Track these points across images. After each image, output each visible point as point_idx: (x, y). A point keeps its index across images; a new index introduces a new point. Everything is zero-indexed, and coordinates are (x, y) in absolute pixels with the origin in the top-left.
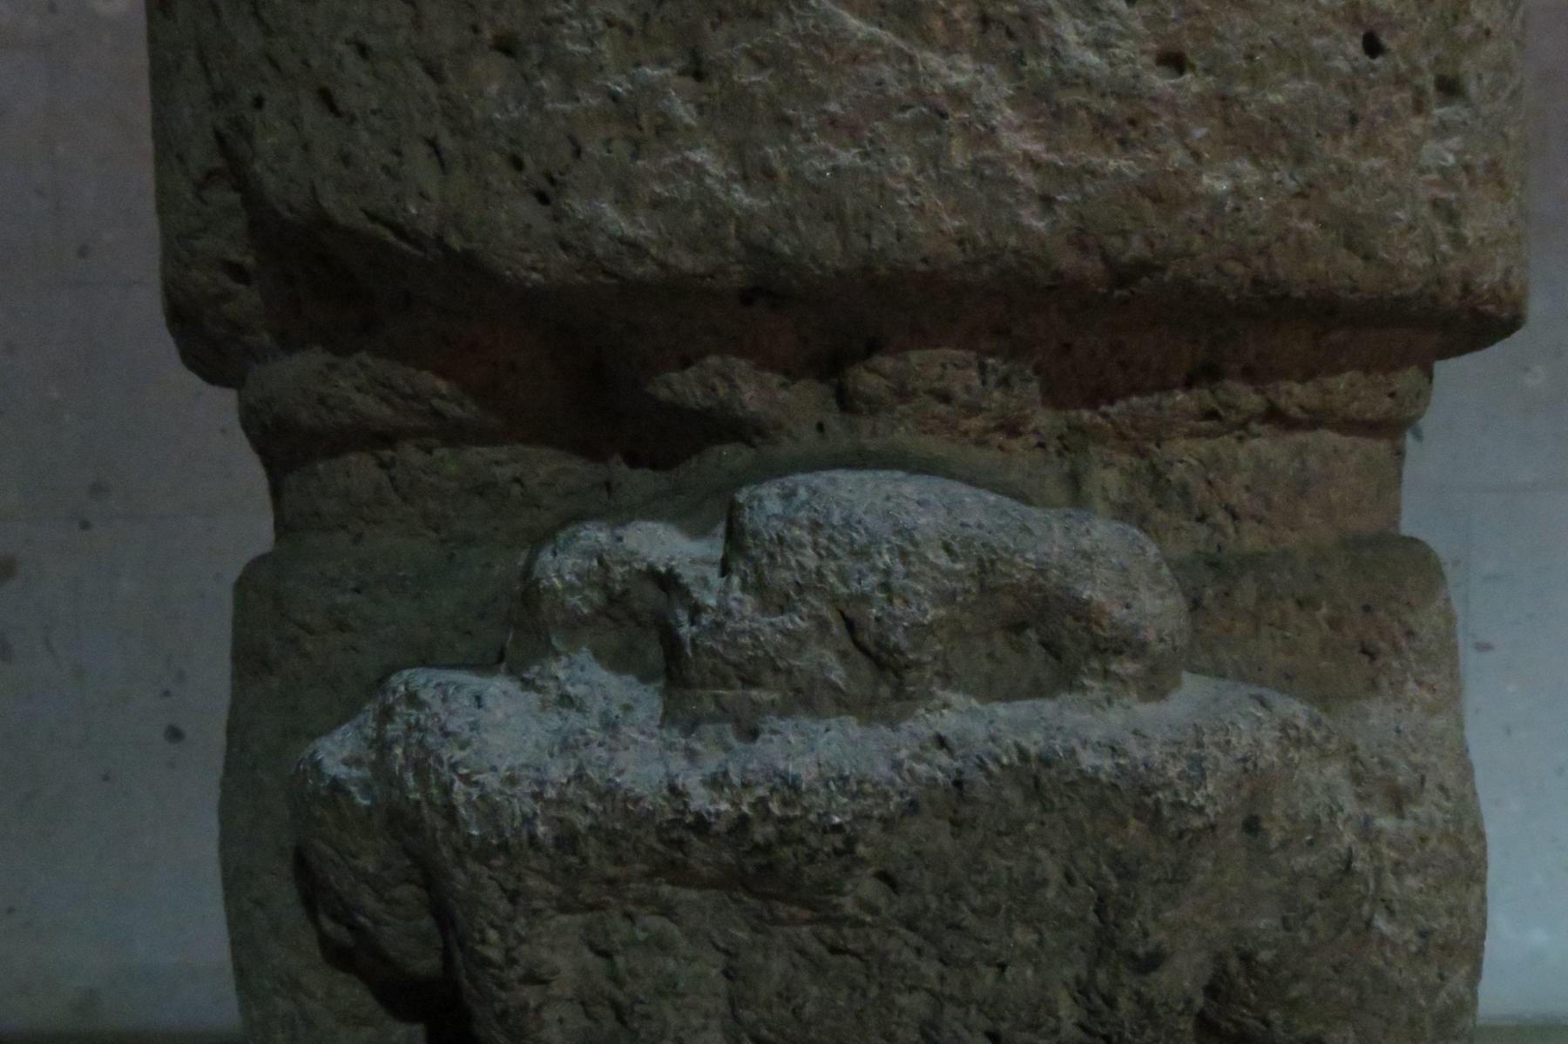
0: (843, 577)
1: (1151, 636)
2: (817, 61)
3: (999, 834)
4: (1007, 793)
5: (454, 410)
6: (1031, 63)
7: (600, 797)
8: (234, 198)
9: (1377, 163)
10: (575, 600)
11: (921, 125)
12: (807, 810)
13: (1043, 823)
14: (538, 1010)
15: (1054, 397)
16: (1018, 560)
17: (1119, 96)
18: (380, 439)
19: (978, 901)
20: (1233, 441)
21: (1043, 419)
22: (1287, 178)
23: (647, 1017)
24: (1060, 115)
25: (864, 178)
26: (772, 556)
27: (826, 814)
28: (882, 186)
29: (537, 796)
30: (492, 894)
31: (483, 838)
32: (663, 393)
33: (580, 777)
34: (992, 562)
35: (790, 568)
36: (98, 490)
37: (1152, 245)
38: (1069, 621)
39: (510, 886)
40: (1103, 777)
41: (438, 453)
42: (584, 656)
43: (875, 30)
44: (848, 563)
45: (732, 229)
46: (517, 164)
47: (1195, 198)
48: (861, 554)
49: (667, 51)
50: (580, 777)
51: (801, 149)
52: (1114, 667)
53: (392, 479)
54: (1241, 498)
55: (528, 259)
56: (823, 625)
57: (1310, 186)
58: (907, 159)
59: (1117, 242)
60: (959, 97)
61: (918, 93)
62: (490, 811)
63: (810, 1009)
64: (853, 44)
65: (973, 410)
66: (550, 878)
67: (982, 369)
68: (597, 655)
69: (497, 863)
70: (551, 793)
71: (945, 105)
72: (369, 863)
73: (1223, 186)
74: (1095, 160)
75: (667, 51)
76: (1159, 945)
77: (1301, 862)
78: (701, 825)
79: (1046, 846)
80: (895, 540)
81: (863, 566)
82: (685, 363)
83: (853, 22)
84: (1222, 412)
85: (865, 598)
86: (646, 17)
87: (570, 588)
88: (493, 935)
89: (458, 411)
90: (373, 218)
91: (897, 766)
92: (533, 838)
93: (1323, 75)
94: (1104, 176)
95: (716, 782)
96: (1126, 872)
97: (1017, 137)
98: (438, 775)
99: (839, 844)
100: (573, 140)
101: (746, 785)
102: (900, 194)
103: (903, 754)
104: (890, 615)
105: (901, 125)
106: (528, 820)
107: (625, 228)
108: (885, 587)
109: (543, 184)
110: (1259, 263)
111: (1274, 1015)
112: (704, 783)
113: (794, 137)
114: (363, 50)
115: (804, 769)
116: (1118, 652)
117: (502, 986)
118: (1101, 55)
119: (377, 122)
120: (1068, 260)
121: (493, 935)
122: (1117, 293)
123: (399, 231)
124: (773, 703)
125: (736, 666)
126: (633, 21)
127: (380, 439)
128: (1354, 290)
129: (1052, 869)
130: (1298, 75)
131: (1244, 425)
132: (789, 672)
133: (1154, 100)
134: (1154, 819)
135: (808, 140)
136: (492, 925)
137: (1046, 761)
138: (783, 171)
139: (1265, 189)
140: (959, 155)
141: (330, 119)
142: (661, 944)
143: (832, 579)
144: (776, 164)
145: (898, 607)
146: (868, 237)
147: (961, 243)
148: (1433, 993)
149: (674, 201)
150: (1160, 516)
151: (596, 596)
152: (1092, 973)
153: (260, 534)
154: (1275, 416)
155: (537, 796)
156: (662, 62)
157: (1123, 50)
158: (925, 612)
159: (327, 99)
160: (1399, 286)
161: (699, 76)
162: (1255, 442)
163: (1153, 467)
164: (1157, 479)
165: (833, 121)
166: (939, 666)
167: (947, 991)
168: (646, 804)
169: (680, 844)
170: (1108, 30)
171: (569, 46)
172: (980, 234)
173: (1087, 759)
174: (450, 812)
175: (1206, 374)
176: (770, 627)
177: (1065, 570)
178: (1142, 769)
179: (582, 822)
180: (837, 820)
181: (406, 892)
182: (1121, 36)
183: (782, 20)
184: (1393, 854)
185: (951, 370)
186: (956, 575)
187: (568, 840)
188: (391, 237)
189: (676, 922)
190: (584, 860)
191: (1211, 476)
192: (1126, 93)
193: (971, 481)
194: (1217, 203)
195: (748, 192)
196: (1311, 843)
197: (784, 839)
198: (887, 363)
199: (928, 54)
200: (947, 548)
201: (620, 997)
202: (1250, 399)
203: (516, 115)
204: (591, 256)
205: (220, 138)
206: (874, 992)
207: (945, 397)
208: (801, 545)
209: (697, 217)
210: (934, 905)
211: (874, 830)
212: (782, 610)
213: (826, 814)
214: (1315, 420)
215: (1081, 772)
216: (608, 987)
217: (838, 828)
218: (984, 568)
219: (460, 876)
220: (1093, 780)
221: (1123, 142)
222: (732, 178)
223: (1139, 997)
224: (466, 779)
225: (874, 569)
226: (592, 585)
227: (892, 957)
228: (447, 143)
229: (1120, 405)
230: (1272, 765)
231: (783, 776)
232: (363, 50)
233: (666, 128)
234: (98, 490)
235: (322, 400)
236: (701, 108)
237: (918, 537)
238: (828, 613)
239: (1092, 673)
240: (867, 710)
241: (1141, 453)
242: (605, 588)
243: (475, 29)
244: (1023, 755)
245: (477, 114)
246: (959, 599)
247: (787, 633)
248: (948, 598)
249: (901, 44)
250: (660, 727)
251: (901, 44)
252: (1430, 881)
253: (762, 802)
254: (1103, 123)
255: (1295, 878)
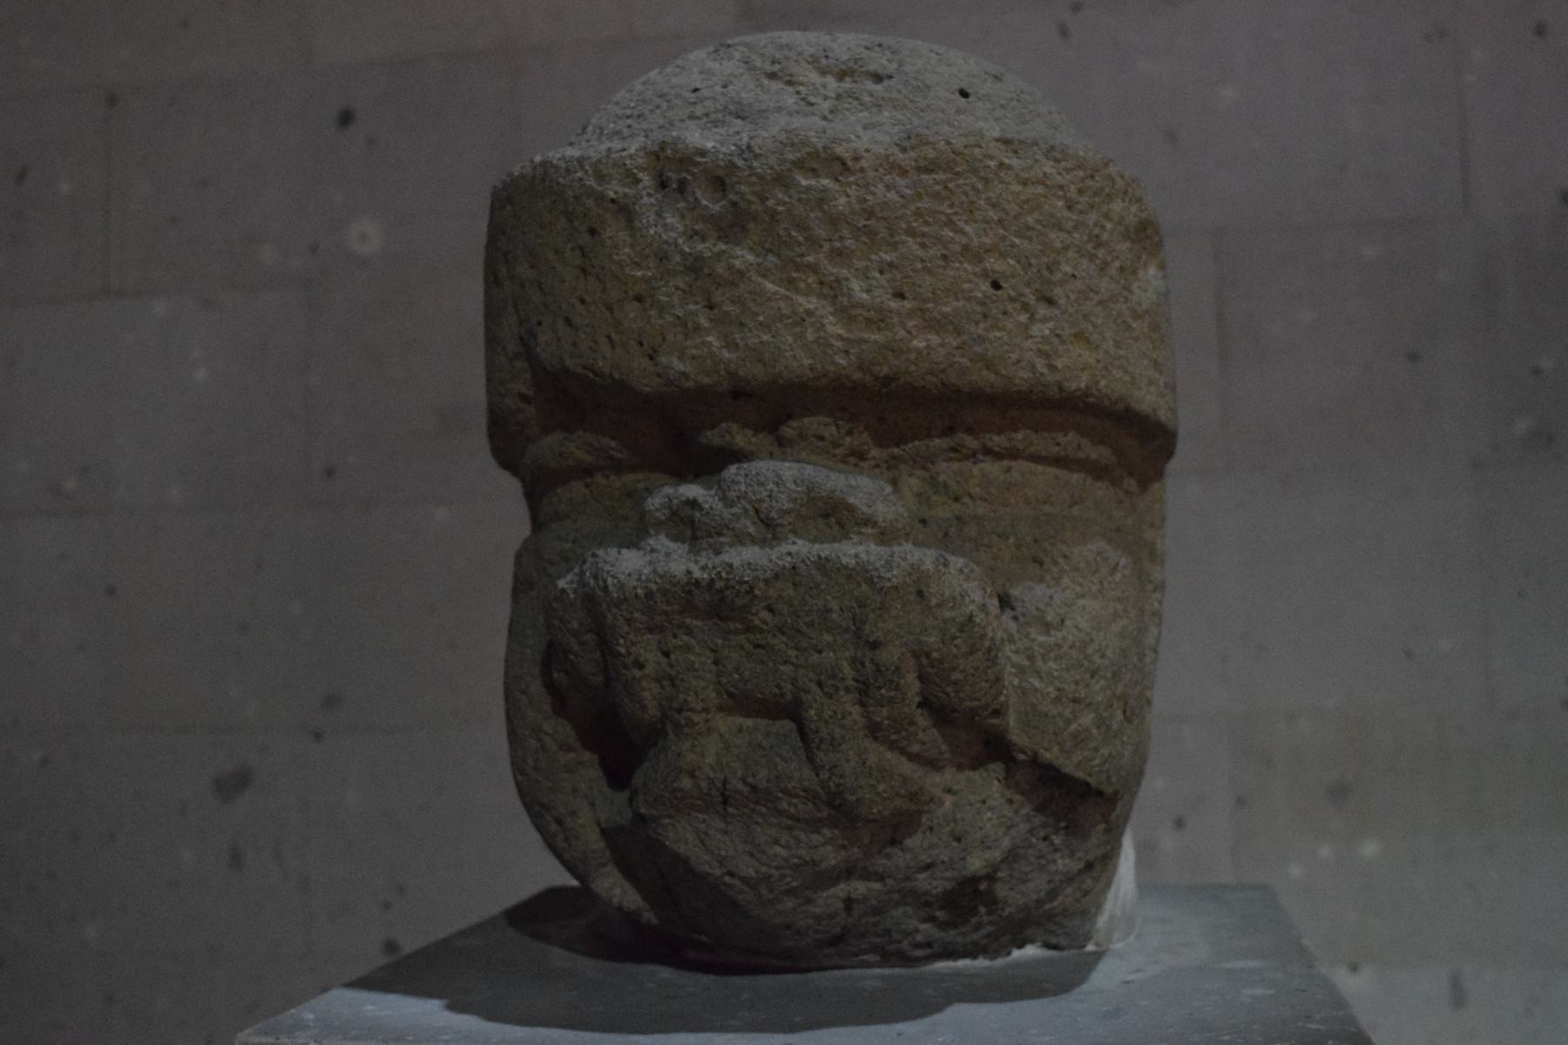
0: (754, 493)
1: (881, 519)
2: (754, 301)
3: (811, 588)
4: (813, 572)
5: (618, 455)
6: (840, 299)
7: (661, 577)
8: (526, 365)
9: (998, 334)
10: (658, 514)
11: (795, 324)
12: (735, 576)
13: (828, 585)
14: (640, 679)
15: (880, 442)
16: (823, 487)
17: (875, 310)
18: (587, 472)
19: (807, 619)
20: (971, 464)
21: (875, 452)
22: (953, 341)
23: (682, 680)
24: (852, 319)
25: (772, 345)
26: (729, 487)
27: (742, 576)
28: (779, 348)
29: (638, 580)
30: (621, 621)
31: (618, 597)
32: (704, 440)
33: (655, 571)
34: (813, 488)
35: (735, 491)
36: (331, 702)
37: (891, 369)
38: (845, 512)
39: (628, 617)
40: (851, 566)
41: (612, 478)
42: (662, 537)
43: (778, 288)
44: (756, 488)
45: (722, 366)
46: (641, 344)
47: (909, 350)
48: (762, 484)
49: (699, 299)
50: (655, 571)
51: (748, 335)
52: (863, 530)
53: (591, 492)
54: (976, 491)
55: (644, 381)
56: (746, 510)
57: (963, 344)
58: (789, 338)
59: (878, 368)
60: (809, 313)
61: (794, 312)
62: (621, 586)
63: (747, 673)
64: (769, 295)
65: (836, 445)
66: (643, 613)
67: (837, 426)
68: (667, 536)
69: (624, 607)
70: (644, 578)
71: (804, 316)
72: (575, 625)
73: (922, 345)
74: (866, 336)
75: (699, 299)
76: (878, 637)
77: (948, 614)
78: (697, 583)
79: (830, 594)
80: (776, 479)
81: (762, 489)
82: (713, 427)
83: (769, 286)
84: (959, 448)
85: (761, 501)
86: (691, 286)
87: (658, 510)
88: (621, 641)
89: (620, 456)
90: (585, 367)
91: (771, 561)
92: (636, 594)
93: (968, 299)
94: (868, 342)
95: (703, 568)
96: (862, 605)
97: (833, 328)
98: (602, 576)
99: (748, 589)
100: (662, 334)
101: (714, 568)
102: (786, 350)
103: (773, 557)
104: (771, 506)
105: (786, 325)
106: (635, 588)
107: (681, 367)
108: (770, 496)
109: (651, 352)
110: (942, 376)
111: (949, 689)
112: (699, 569)
113: (746, 330)
114: (583, 301)
115: (736, 562)
116: (866, 525)
117: (625, 666)
118: (868, 295)
119: (587, 330)
120: (857, 376)
121: (621, 641)
122: (884, 390)
123: (596, 374)
124: (728, 543)
125: (714, 528)
126: (686, 289)
127: (587, 472)
128: (992, 387)
129: (834, 605)
130: (957, 299)
131: (974, 455)
132: (733, 529)
133: (890, 312)
134: (870, 581)
135: (751, 331)
136: (622, 637)
137: (827, 559)
138: (741, 344)
139: (942, 345)
140: (810, 335)
141: (568, 329)
142: (687, 648)
143: (750, 494)
144: (738, 341)
145: (774, 503)
146: (774, 367)
147: (811, 369)
148: (1068, 722)
149: (700, 357)
150: (935, 498)
151: (666, 512)
152: (856, 653)
153: (526, 530)
154: (988, 451)
155: (638, 580)
156: (697, 303)
157: (877, 292)
158: (784, 505)
159: (568, 321)
160: (1016, 385)
161: (711, 308)
162: (982, 465)
163: (931, 477)
164: (933, 481)
165: (761, 324)
166: (790, 527)
167: (799, 663)
168: (678, 578)
169: (689, 592)
170: (870, 285)
171: (661, 297)
172: (819, 366)
173: (845, 560)
174: (606, 588)
175: (949, 431)
176: (727, 514)
177: (842, 491)
178: (866, 564)
179: (654, 587)
180: (746, 579)
181: (589, 637)
182: (876, 287)
183: (742, 286)
184: (1042, 651)
185: (822, 427)
186: (797, 492)
187: (649, 595)
188: (591, 375)
189: (693, 638)
190: (656, 602)
191: (958, 478)
192: (880, 310)
193: (808, 463)
194: (919, 352)
195: (729, 352)
196: (952, 607)
197: (727, 588)
198: (794, 424)
199: (798, 297)
200: (795, 482)
201: (673, 673)
202: (972, 443)
203: (640, 325)
204: (668, 379)
205: (521, 338)
206: (771, 664)
207: (822, 439)
208: (740, 483)
209: (709, 362)
210: (789, 621)
211: (762, 585)
212: (732, 507)
213: (742, 576)
214: (1014, 454)
215: (841, 564)
216: (668, 669)
217: (746, 582)
218: (809, 490)
219: (609, 616)
220: (846, 567)
221: (879, 328)
222: (723, 347)
223: (872, 661)
224: (613, 577)
225: (766, 490)
226: (665, 508)
227: (777, 647)
228: (614, 336)
229: (910, 445)
230: (928, 570)
231: (727, 564)
232: (583, 301)
233: (697, 328)
234: (331, 702)
235: (561, 454)
236: (711, 320)
237: (784, 478)
238: (748, 507)
239: (854, 532)
240: (763, 543)
241: (925, 469)
242: (670, 508)
243: (626, 292)
244: (820, 557)
245: (626, 325)
246: (799, 501)
247: (733, 515)
248: (795, 500)
249: (788, 293)
250: (687, 554)
251: (788, 293)
252: (1063, 666)
253: (719, 573)
254: (869, 321)
255: (945, 621)
